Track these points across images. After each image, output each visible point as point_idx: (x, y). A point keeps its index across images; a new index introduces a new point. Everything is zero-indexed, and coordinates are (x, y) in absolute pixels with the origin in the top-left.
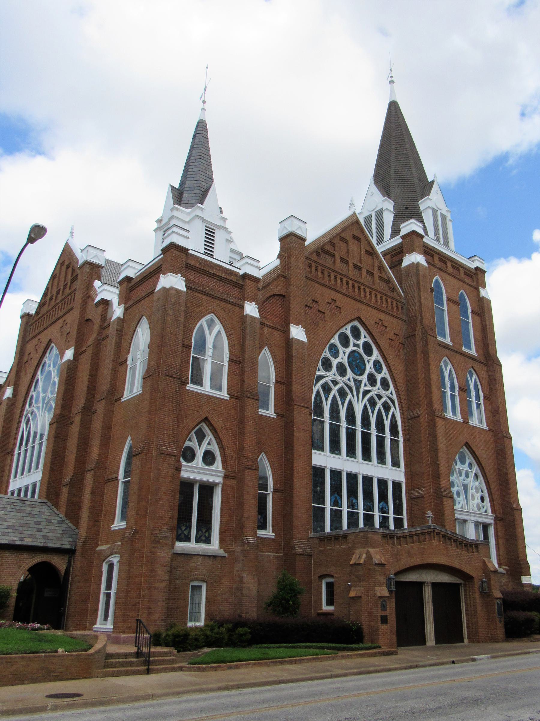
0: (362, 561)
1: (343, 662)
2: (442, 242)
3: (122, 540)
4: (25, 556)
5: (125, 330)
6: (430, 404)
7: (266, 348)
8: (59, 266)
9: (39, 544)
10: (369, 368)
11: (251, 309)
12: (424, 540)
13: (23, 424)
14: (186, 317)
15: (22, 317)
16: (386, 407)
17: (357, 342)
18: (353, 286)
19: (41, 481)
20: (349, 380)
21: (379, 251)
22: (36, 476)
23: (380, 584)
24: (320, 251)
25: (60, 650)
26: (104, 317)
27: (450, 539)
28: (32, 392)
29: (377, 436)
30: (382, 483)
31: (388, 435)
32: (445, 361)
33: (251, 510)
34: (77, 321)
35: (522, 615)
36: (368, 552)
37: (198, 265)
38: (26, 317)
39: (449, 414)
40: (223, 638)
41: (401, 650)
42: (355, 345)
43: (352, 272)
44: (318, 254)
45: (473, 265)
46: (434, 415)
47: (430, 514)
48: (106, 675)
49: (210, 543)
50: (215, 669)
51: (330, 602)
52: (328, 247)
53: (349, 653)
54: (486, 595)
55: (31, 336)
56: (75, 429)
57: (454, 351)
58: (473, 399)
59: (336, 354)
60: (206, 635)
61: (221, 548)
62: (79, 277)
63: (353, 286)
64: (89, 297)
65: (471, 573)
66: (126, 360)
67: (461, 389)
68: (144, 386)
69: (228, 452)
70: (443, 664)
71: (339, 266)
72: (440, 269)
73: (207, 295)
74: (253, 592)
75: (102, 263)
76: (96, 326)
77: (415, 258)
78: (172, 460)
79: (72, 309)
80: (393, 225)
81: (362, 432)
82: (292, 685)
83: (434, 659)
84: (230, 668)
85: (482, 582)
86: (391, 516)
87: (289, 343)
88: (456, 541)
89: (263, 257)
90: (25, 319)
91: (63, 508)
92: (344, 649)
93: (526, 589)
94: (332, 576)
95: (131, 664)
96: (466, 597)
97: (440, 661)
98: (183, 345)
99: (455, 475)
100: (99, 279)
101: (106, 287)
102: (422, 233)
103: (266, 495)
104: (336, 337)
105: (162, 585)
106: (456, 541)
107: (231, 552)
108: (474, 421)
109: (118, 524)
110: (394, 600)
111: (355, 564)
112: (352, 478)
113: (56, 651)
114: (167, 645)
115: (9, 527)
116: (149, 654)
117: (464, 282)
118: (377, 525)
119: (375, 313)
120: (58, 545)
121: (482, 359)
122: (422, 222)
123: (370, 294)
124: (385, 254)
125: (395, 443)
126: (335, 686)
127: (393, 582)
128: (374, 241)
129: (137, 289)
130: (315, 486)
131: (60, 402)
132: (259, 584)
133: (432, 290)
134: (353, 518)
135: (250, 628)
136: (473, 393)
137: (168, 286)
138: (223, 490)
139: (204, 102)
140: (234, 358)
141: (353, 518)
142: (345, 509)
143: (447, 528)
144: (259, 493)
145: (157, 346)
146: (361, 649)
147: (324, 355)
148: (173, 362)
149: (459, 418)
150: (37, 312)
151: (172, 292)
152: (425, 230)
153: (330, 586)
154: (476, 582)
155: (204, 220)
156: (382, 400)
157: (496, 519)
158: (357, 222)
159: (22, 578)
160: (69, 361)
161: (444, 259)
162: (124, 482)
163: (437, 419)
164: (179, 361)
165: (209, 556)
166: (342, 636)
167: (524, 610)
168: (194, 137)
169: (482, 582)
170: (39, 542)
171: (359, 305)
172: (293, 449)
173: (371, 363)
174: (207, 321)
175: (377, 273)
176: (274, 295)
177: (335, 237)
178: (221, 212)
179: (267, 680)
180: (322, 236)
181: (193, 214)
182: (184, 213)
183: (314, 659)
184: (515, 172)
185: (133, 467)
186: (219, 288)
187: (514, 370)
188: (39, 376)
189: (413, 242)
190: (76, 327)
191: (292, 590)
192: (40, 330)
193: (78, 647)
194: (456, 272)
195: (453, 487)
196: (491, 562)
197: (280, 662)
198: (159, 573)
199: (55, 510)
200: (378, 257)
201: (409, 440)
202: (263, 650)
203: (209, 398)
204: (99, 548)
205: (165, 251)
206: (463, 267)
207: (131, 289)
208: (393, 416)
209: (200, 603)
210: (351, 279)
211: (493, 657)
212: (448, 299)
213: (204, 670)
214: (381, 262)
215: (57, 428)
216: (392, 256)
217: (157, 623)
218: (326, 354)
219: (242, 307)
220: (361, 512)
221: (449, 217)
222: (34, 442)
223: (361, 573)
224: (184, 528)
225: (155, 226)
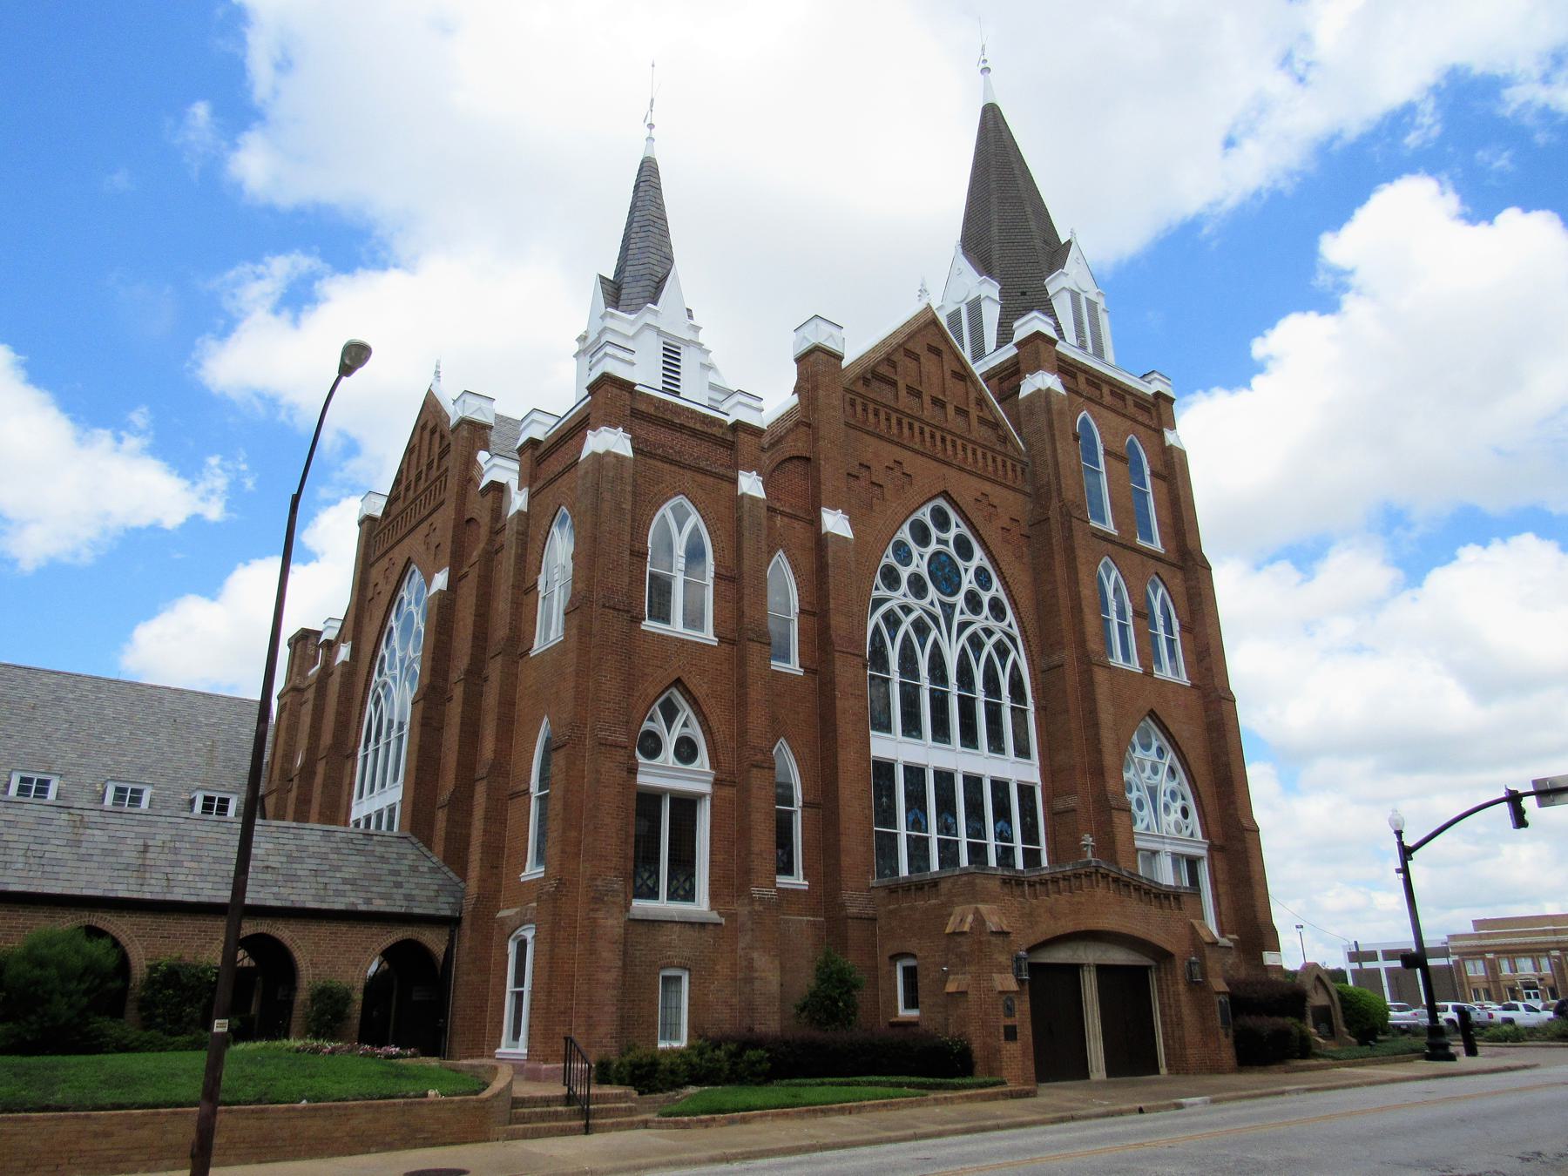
0: (966, 928)
1: (937, 1110)
2: (1090, 350)
3: (538, 899)
4: (375, 930)
5: (531, 533)
6: (1082, 642)
7: (781, 552)
9: (397, 910)
10: (968, 582)
11: (750, 484)
12: (1080, 888)
13: (370, 707)
14: (634, 503)
15: (361, 523)
16: (1002, 651)
17: (943, 536)
18: (933, 436)
19: (402, 801)
20: (932, 603)
21: (978, 373)
22: (393, 795)
23: (1002, 969)
24: (869, 376)
25: (431, 1093)
26: (497, 512)
27: (1127, 885)
28: (383, 650)
29: (987, 703)
30: (1000, 787)
31: (1006, 701)
33: (763, 839)
34: (451, 524)
35: (1267, 1024)
36: (977, 912)
37: (652, 411)
38: (367, 522)
39: (1117, 660)
40: (720, 1070)
41: (1044, 1088)
42: (939, 541)
43: (929, 412)
44: (866, 382)
45: (1149, 389)
46: (1090, 662)
47: (1088, 840)
48: (513, 1136)
49: (693, 900)
50: (706, 1124)
51: (911, 1002)
52: (884, 370)
53: (948, 1094)
54: (1197, 986)
55: (378, 554)
56: (455, 710)
57: (1125, 547)
58: (1161, 631)
59: (906, 559)
60: (690, 1064)
61: (712, 909)
62: (452, 448)
63: (933, 436)
64: (470, 480)
65: (1169, 948)
66: (535, 585)
67: (1136, 613)
68: (566, 629)
69: (719, 737)
70: (1121, 1113)
71: (905, 401)
72: (1090, 399)
73: (672, 462)
74: (772, 987)
75: (490, 420)
76: (484, 531)
77: (1044, 381)
78: (620, 756)
79: (442, 503)
80: (1000, 324)
81: (960, 696)
82: (842, 1152)
83: (1107, 1106)
84: (732, 1122)
85: (1190, 963)
86: (1018, 845)
87: (821, 541)
88: (1138, 889)
89: (771, 397)
90: (365, 525)
91: (439, 845)
92: (938, 1087)
93: (1274, 976)
94: (914, 956)
95: (556, 1116)
96: (1160, 991)
97: (1117, 1108)
98: (632, 553)
99: (1132, 771)
100: (487, 449)
101: (497, 461)
102: (1055, 336)
103: (791, 813)
104: (906, 527)
105: (611, 977)
106: (1138, 889)
107: (731, 917)
108: (1165, 672)
109: (532, 871)
110: (1027, 998)
111: (954, 933)
112: (944, 779)
113: (426, 1095)
114: (621, 1083)
115: (345, 881)
116: (588, 1099)
117: (1135, 420)
118: (992, 861)
119: (975, 483)
120: (429, 910)
121: (1173, 558)
122: (1053, 316)
123: (964, 449)
124: (988, 376)
125: (1019, 715)
126: (921, 1154)
127: (1024, 965)
128: (967, 355)
129: (547, 458)
130: (878, 797)
131: (429, 664)
132: (782, 968)
133: (1076, 438)
134: (948, 851)
135: (768, 1050)
136: (1160, 621)
137: (601, 450)
138: (712, 806)
139: (651, 126)
140: (723, 571)
141: (948, 851)
142: (933, 835)
143: (1122, 865)
144: (779, 811)
145: (587, 559)
146: (970, 1087)
147: (884, 561)
148: (617, 588)
149: (1135, 666)
150: (386, 513)
151: (607, 459)
152: (1058, 329)
153: (910, 973)
154: (1178, 962)
155: (659, 332)
156: (994, 639)
157: (1211, 849)
158: (934, 322)
159: (373, 968)
160: (440, 591)
161: (1096, 380)
162: (540, 798)
163: (1096, 669)
164: (627, 580)
165: (692, 924)
166: (933, 1063)
167: (1271, 1014)
168: (637, 187)
169: (1190, 963)
170: (399, 906)
171: (945, 469)
172: (835, 731)
173: (971, 572)
174: (673, 509)
175: (974, 412)
176: (791, 459)
177: (895, 350)
178: (691, 317)
179: (797, 1143)
180: (873, 350)
181: (641, 324)
182: (624, 322)
183: (885, 1105)
184: (1214, 244)
185: (553, 769)
186: (694, 450)
187: (1234, 589)
189: (1037, 352)
190: (450, 534)
191: (843, 982)
192: (391, 542)
193: (462, 1088)
194: (1119, 404)
195: (1130, 791)
196: (1206, 927)
197: (822, 1111)
198: (605, 955)
199: (424, 849)
200: (974, 382)
201: (1045, 708)
202: (794, 1090)
203: (683, 643)
204: (501, 914)
205: (593, 389)
206: (1131, 394)
207: (539, 461)
208: (1015, 665)
209: (678, 1008)
210: (928, 424)
211: (1213, 1102)
212: (1107, 453)
213: (686, 1126)
214: (981, 391)
215: (425, 710)
216: (1002, 380)
217: (602, 1042)
218: (889, 558)
219: (734, 482)
220: (963, 840)
221: (1102, 305)
222: (388, 735)
223: (965, 949)
224: (646, 875)
225: (576, 347)
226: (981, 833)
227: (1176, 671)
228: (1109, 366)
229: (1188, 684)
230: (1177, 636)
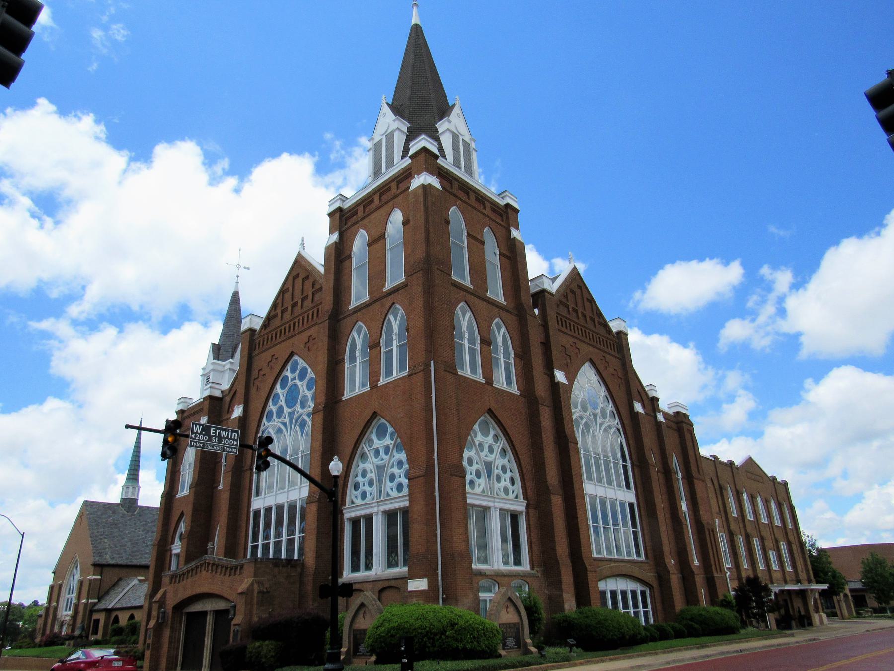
8: (291, 278)
32: (497, 324)
52: (564, 300)
102: (436, 151)
149: (480, 378)
161: (466, 188)
188: (278, 389)
206: (488, 201)
212: (469, 235)
221: (473, 145)
226: (597, 522)
227: (509, 382)
228: (479, 181)
229: (518, 393)
230: (512, 361)
